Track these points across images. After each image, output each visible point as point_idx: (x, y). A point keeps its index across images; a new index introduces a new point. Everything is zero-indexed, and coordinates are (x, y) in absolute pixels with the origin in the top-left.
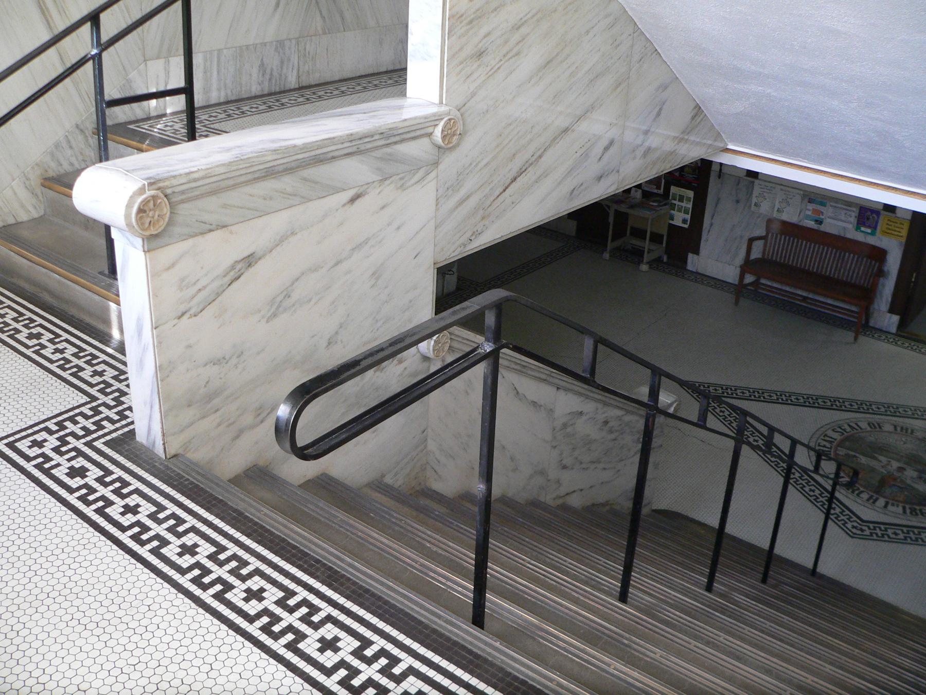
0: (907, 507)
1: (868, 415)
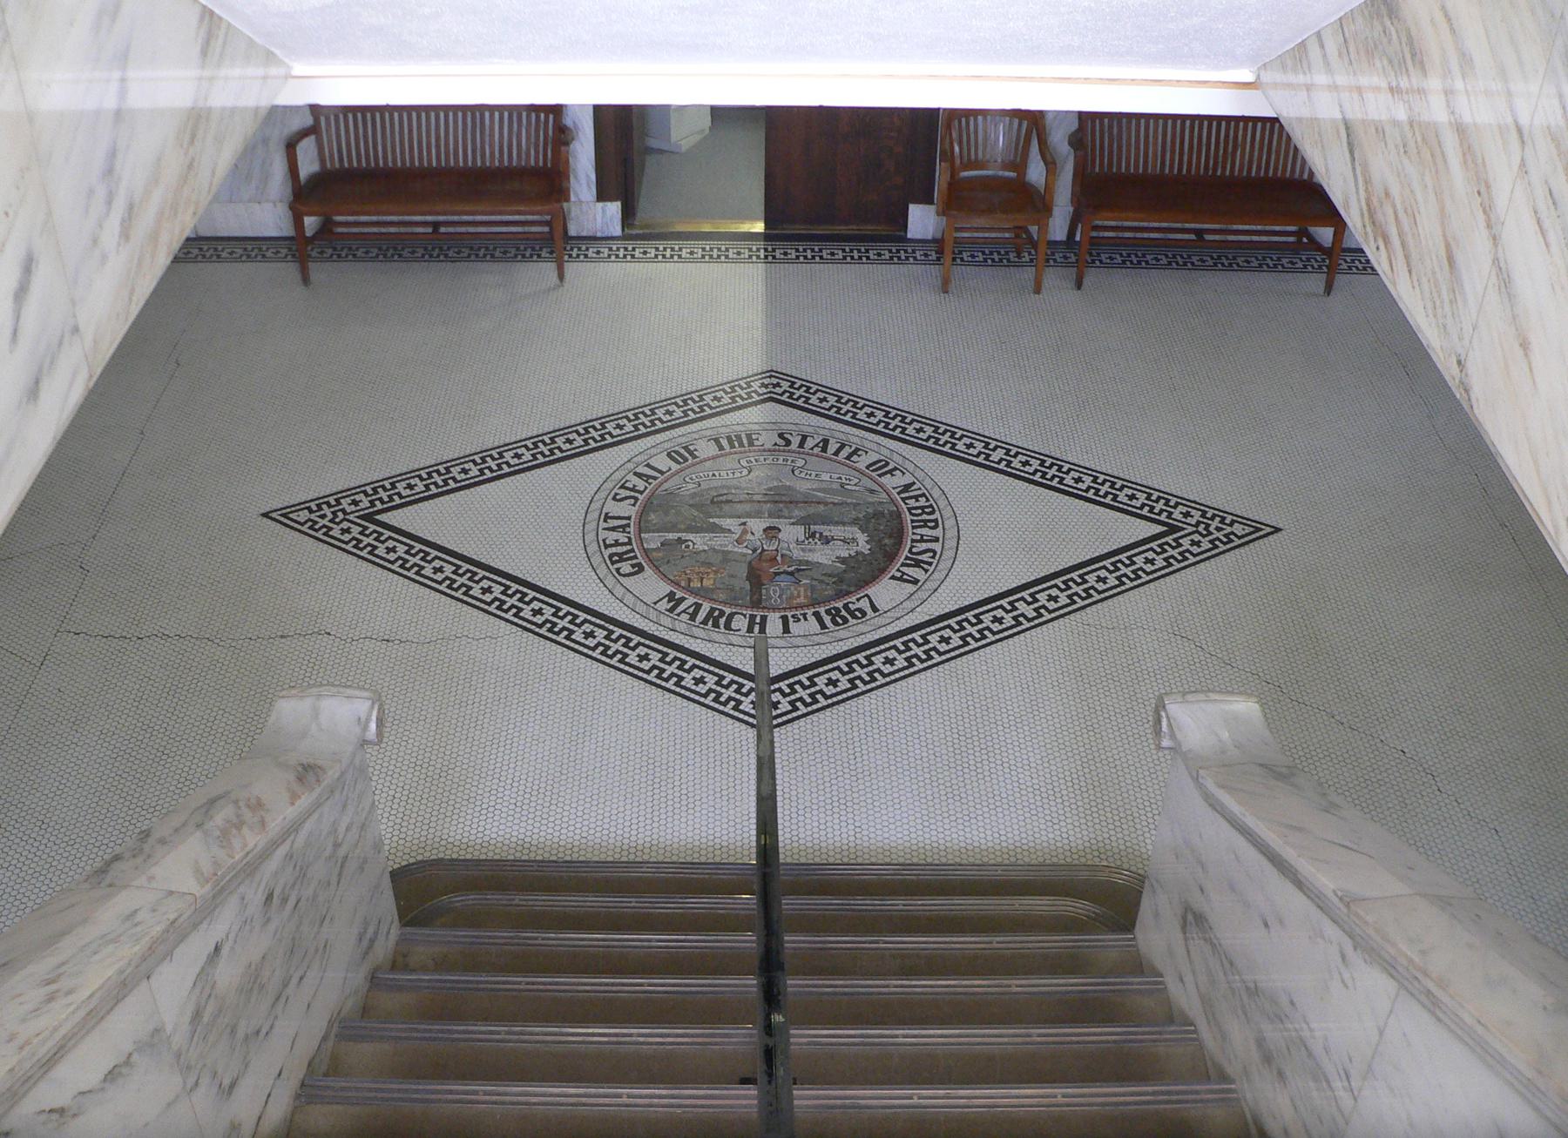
0: (822, 610)
1: (659, 437)
